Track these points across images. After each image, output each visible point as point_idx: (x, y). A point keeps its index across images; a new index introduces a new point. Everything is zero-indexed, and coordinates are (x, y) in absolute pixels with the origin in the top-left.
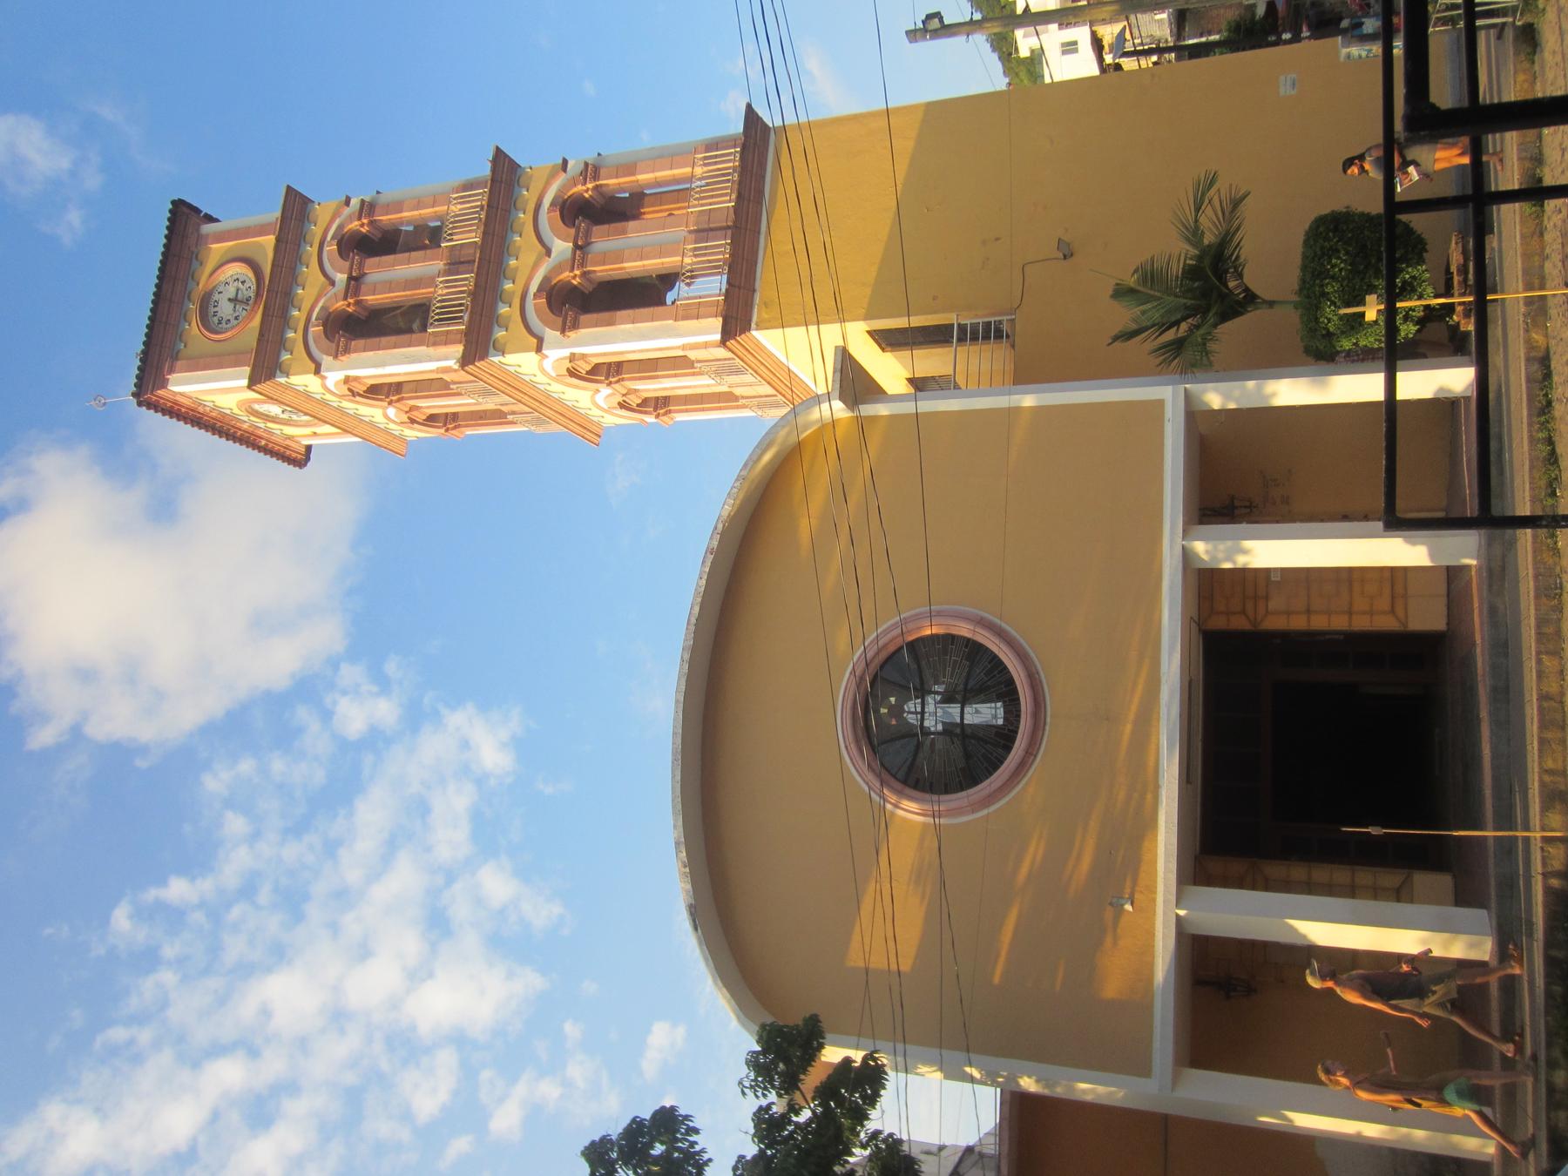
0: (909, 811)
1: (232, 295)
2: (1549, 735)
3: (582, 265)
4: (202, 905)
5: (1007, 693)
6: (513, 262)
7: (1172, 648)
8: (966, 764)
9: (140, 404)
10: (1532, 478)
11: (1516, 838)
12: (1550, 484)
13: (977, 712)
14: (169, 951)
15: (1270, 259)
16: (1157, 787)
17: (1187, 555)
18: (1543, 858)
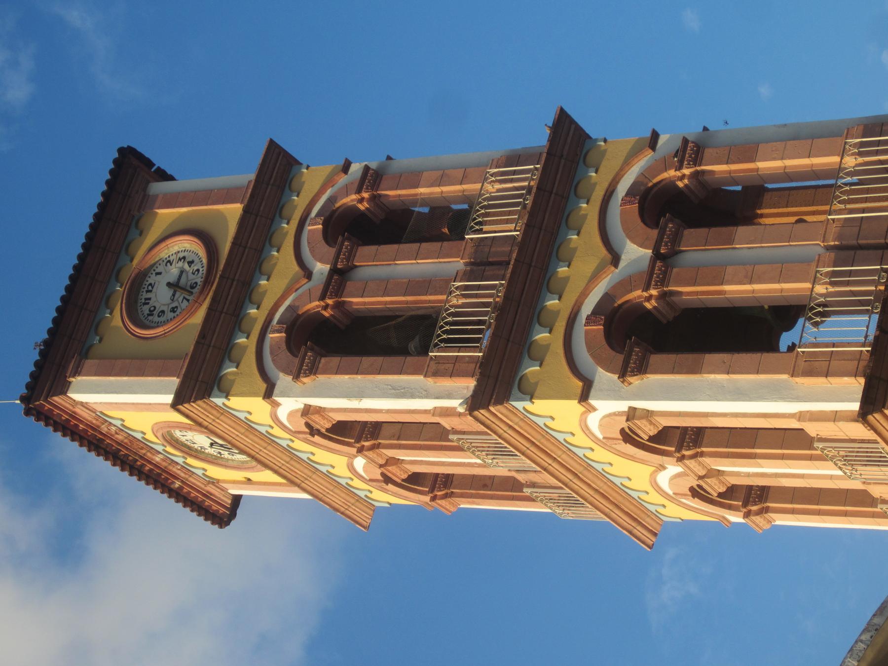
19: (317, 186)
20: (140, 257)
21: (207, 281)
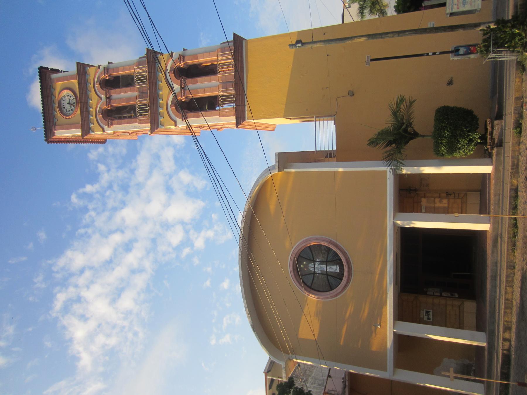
0: (312, 297)
1: (68, 102)
2: (507, 311)
3: (185, 95)
4: (98, 192)
5: (339, 262)
6: (161, 92)
7: (390, 251)
8: (327, 284)
9: (48, 143)
10: (508, 230)
11: (493, 382)
12: (514, 233)
13: (331, 268)
14: (91, 206)
15: (423, 120)
16: (387, 294)
17: (395, 224)
18: (502, 345)
19: (94, 76)
20: (57, 98)
21: (77, 102)
